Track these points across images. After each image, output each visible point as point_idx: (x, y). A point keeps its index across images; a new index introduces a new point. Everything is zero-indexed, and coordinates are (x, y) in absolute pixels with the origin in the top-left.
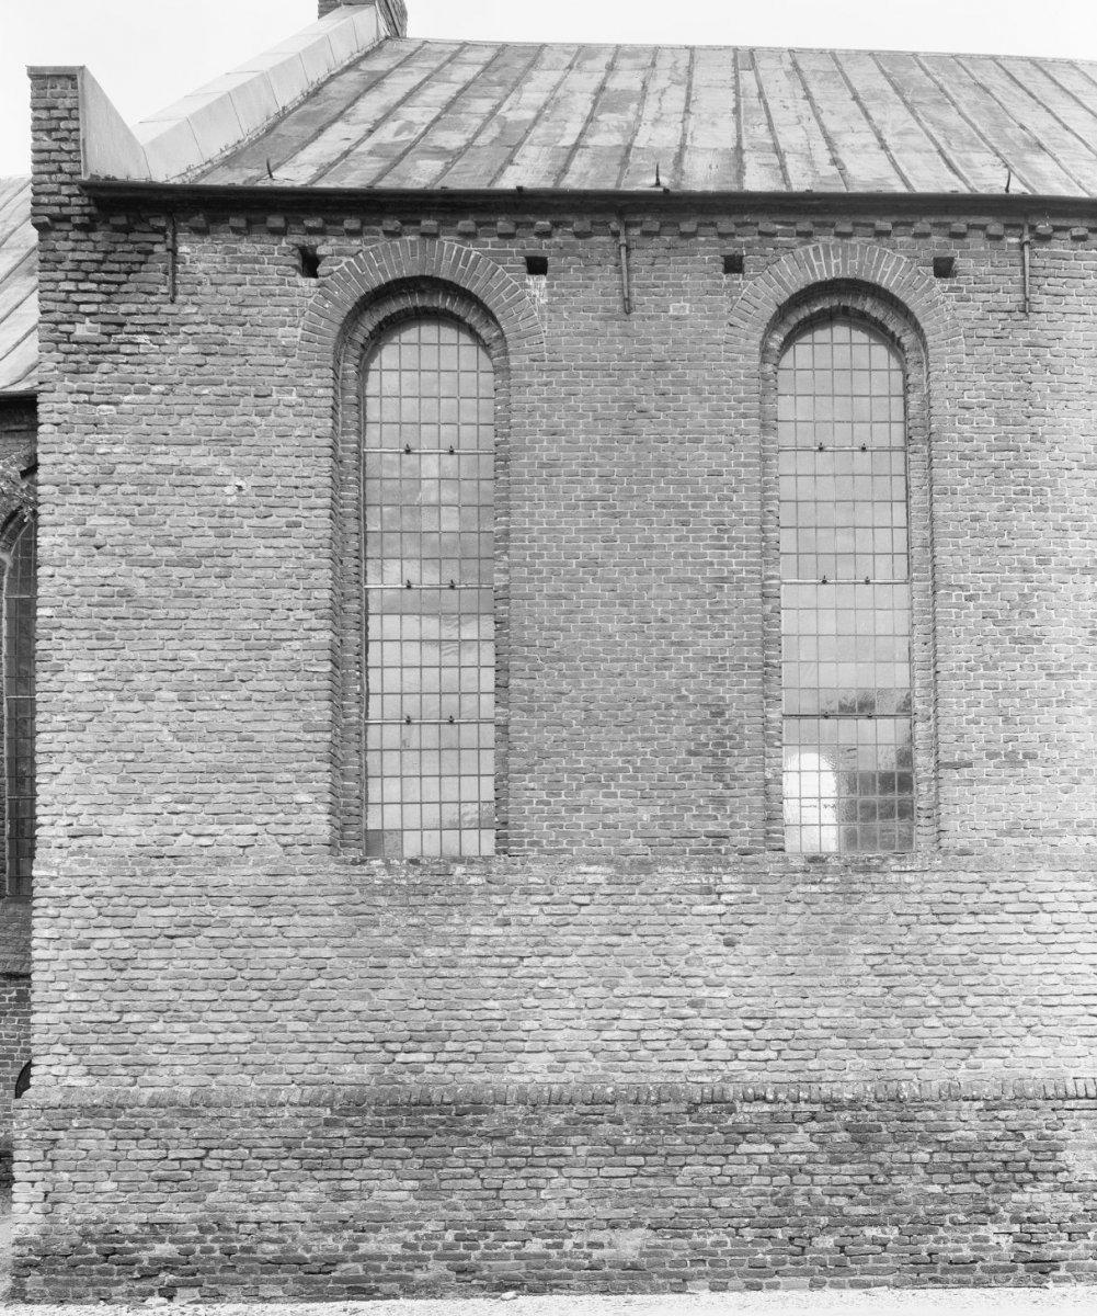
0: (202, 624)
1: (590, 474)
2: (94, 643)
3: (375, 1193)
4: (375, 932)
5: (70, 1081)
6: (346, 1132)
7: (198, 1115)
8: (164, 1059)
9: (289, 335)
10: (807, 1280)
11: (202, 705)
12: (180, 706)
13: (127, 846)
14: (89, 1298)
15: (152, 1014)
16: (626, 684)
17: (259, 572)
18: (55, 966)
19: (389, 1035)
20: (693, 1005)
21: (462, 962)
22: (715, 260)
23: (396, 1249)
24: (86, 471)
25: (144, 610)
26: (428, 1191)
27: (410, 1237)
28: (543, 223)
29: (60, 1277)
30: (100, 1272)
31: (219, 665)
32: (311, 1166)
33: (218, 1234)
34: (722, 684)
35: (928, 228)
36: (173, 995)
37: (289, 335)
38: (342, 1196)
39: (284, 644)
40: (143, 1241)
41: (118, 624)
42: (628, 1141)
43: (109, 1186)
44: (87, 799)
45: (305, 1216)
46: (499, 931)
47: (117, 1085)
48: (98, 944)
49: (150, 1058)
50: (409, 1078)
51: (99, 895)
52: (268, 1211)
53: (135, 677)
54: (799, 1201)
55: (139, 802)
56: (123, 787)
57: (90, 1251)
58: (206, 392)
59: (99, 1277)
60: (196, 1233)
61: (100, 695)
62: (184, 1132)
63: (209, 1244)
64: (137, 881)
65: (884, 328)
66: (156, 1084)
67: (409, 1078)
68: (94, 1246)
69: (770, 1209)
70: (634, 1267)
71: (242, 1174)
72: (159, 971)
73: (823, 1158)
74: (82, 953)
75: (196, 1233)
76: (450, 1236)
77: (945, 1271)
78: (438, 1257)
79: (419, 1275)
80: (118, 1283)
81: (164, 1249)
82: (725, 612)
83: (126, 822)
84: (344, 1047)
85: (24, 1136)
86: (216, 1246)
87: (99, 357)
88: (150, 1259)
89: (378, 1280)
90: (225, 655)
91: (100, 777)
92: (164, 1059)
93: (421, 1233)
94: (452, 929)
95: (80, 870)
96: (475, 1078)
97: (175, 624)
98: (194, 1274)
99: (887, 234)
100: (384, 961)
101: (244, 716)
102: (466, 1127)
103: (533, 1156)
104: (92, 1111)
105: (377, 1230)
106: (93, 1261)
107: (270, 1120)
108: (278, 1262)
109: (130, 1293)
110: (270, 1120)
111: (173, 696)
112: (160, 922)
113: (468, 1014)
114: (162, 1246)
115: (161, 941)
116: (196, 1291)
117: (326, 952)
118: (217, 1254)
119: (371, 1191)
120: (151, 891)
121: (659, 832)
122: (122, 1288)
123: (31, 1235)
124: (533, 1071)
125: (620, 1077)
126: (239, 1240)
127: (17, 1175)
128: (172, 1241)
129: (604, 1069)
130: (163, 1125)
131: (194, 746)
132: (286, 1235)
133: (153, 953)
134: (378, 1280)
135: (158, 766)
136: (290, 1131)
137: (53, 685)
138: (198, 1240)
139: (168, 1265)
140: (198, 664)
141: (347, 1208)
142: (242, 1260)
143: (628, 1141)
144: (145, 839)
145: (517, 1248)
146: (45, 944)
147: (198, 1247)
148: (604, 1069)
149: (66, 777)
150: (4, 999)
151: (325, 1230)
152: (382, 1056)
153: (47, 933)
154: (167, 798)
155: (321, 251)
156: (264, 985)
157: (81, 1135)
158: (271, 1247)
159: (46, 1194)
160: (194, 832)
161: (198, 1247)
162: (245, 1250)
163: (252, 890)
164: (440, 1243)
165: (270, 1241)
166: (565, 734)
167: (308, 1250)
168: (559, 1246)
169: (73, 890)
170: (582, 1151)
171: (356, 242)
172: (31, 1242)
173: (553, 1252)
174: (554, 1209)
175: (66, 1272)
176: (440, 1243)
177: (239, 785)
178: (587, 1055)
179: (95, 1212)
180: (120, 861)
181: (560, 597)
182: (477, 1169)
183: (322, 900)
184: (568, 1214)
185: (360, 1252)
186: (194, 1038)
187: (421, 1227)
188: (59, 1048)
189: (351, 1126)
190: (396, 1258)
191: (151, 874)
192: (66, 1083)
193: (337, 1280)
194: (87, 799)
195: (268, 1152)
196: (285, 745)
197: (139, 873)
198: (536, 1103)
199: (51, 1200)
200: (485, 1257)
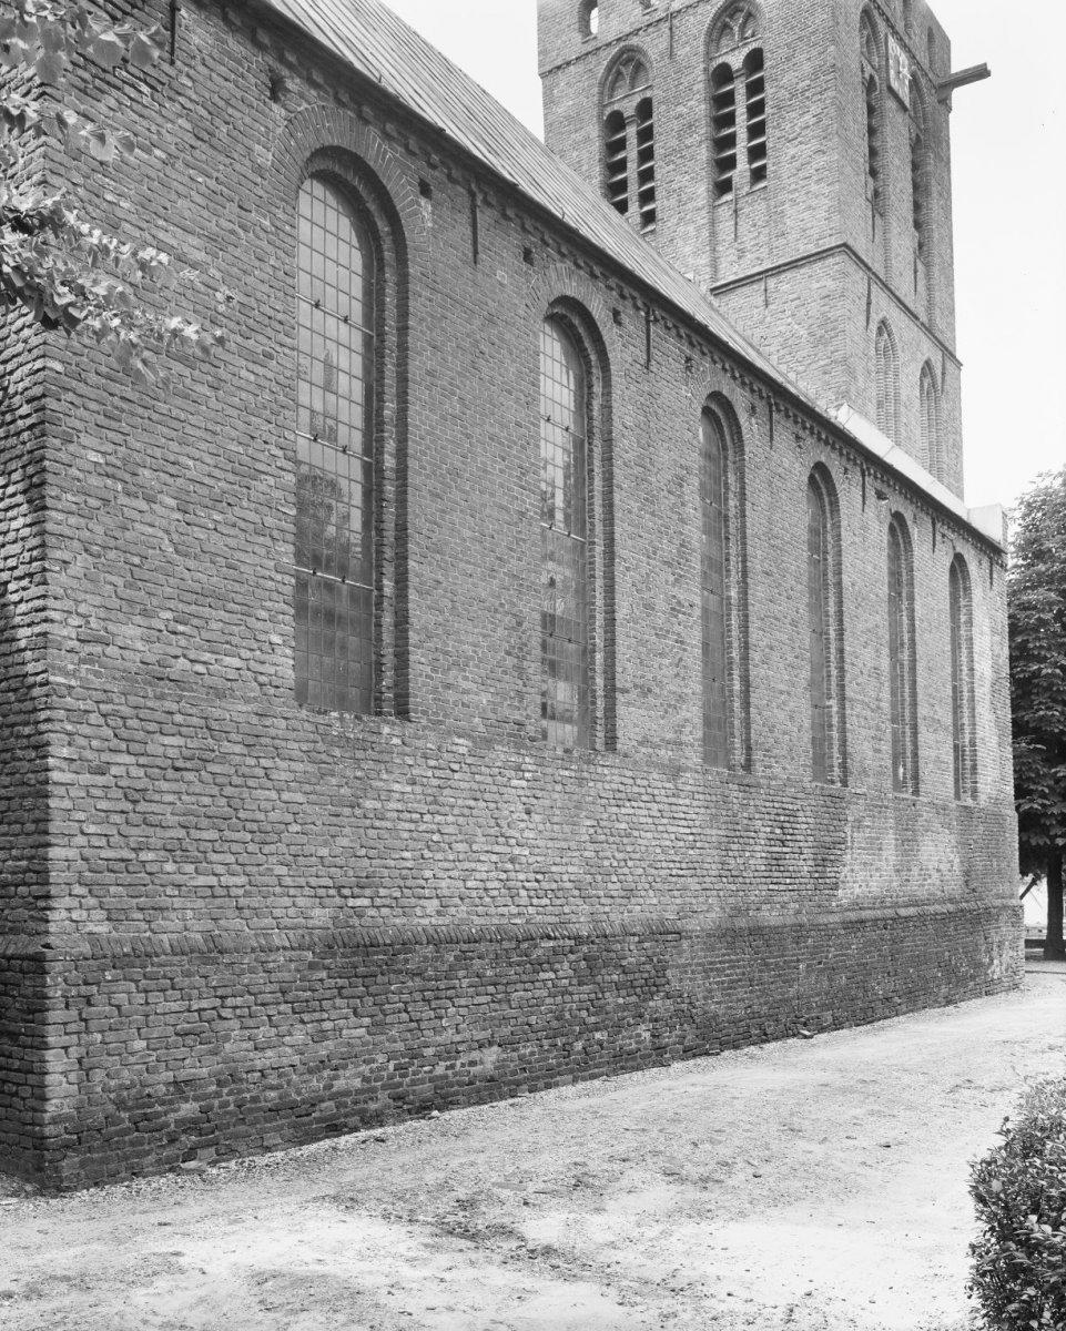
0: (198, 433)
1: (454, 394)
2: (101, 419)
3: (344, 1032)
4: (334, 781)
5: (91, 927)
6: (324, 974)
7: (215, 962)
8: (177, 903)
9: (266, 158)
10: (571, 1077)
11: (197, 520)
12: (178, 516)
13: (133, 662)
14: (123, 1175)
15: (162, 853)
16: (473, 584)
17: (244, 395)
18: (74, 792)
19: (343, 881)
20: (512, 861)
21: (389, 815)
22: (518, 247)
23: (357, 1083)
24: (94, 215)
25: (148, 399)
26: (377, 1027)
27: (365, 1069)
28: (435, 158)
29: (95, 1156)
30: (132, 1144)
31: (211, 482)
32: (300, 1010)
33: (233, 1086)
34: (521, 600)
35: (614, 286)
36: (181, 833)
37: (266, 158)
38: (321, 1036)
39: (263, 477)
40: (171, 1102)
41: (125, 406)
42: (489, 973)
43: (140, 1045)
44: (98, 600)
45: (296, 1059)
46: (409, 789)
47: (132, 932)
48: (114, 770)
49: (163, 901)
50: (355, 921)
51: (115, 713)
52: (268, 1058)
53: (140, 471)
54: (567, 1016)
55: (145, 613)
56: (128, 593)
57: (123, 1121)
58: (200, 180)
59: (131, 1149)
60: (214, 1088)
61: (109, 482)
62: (203, 981)
63: (225, 1098)
64: (150, 704)
65: (381, 269)
66: (169, 931)
67: (355, 921)
68: (127, 1115)
69: (555, 1024)
70: (492, 1079)
71: (251, 1023)
72: (168, 802)
73: (575, 981)
74: (100, 780)
75: (214, 1088)
76: (391, 1066)
77: (627, 1060)
78: (384, 1087)
79: (373, 1106)
80: (148, 1153)
81: (188, 1109)
82: (524, 541)
83: (130, 632)
84: (312, 892)
85: (59, 993)
86: (231, 1098)
87: (106, 87)
88: (176, 1121)
89: (346, 1116)
90: (217, 473)
91: (110, 578)
92: (177, 903)
93: (374, 1066)
94: (382, 784)
95: (97, 683)
96: (397, 921)
97: (175, 424)
98: (213, 1132)
99: (596, 277)
100: (339, 810)
101: (230, 541)
102: (399, 966)
103: (438, 989)
104: (118, 962)
105: (345, 1067)
106: (125, 1132)
107: (272, 965)
108: (275, 1110)
109: (159, 1162)
110: (272, 965)
111: (173, 503)
112: (171, 752)
113: (392, 863)
114: (188, 1106)
115: (170, 773)
116: (213, 1150)
117: (300, 798)
118: (232, 1107)
119: (341, 1030)
120: (159, 716)
121: (491, 715)
122: (151, 1158)
123: (66, 1110)
124: (427, 916)
125: (477, 920)
126: (249, 1091)
127: (51, 1040)
128: (196, 1099)
129: (468, 913)
130: (188, 974)
131: (191, 564)
132: (283, 1081)
133: (165, 786)
134: (346, 1116)
135: (161, 578)
136: (286, 976)
137: (62, 456)
138: (218, 1095)
139: (190, 1126)
140: (192, 474)
141: (326, 1048)
142: (251, 1110)
143: (489, 973)
144: (151, 658)
145: (431, 1072)
146: (64, 765)
147: (216, 1102)
148: (468, 913)
149: (76, 569)
150: (1062, 713)
151: (310, 1071)
152: (338, 901)
153: (65, 752)
154: (169, 615)
155: (290, 84)
156: (254, 827)
157: (114, 989)
158: (273, 1094)
159: (80, 1061)
160: (192, 657)
161: (216, 1102)
162: (255, 1099)
163: (245, 728)
164: (385, 1074)
165: (272, 1088)
166: (440, 619)
167: (299, 1094)
168: (452, 1067)
169: (90, 705)
170: (465, 982)
171: (313, 92)
172: (68, 1118)
173: (450, 1072)
174: (449, 1036)
175: (101, 1149)
176: (385, 1074)
177: (227, 615)
178: (457, 901)
179: (127, 1076)
180: (128, 676)
181: (438, 496)
182: (406, 1003)
183: (296, 746)
184: (458, 1038)
185: (334, 1090)
186: (201, 881)
187: (373, 1061)
188: (78, 890)
189: (327, 968)
190: (358, 1092)
191: (161, 697)
192: (87, 930)
193: (318, 1120)
194: (98, 600)
195: (268, 998)
196: (261, 581)
197: (151, 694)
198: (438, 941)
199: (85, 1067)
200: (413, 1083)
